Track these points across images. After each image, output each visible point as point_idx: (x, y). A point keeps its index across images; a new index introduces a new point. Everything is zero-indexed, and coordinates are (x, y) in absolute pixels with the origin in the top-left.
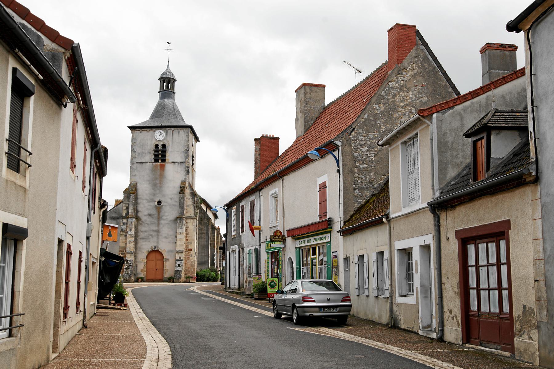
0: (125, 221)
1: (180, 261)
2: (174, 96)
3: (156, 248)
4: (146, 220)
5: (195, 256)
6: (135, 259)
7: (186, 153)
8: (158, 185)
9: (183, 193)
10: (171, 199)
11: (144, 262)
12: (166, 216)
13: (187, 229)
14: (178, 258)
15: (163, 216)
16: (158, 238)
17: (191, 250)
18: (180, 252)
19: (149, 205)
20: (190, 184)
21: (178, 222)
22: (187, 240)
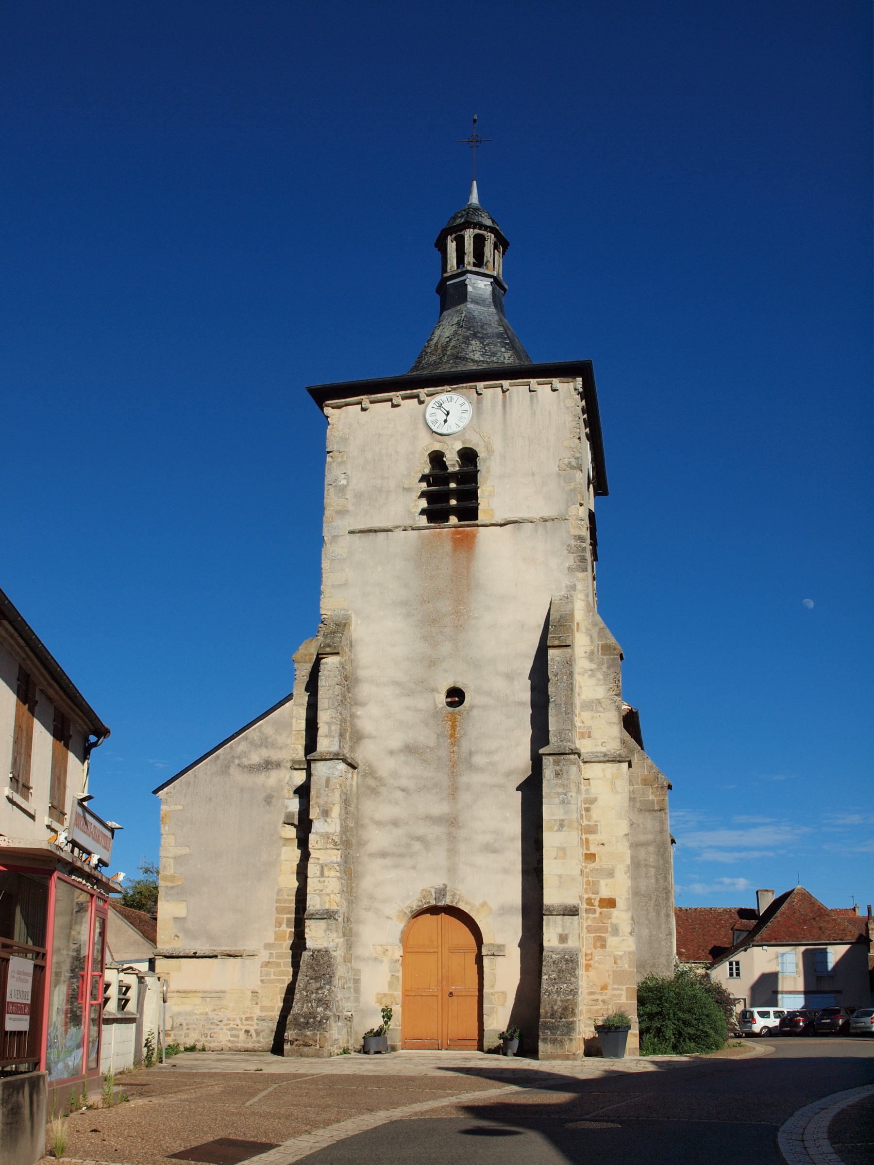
13: (587, 810)
16: (452, 852)
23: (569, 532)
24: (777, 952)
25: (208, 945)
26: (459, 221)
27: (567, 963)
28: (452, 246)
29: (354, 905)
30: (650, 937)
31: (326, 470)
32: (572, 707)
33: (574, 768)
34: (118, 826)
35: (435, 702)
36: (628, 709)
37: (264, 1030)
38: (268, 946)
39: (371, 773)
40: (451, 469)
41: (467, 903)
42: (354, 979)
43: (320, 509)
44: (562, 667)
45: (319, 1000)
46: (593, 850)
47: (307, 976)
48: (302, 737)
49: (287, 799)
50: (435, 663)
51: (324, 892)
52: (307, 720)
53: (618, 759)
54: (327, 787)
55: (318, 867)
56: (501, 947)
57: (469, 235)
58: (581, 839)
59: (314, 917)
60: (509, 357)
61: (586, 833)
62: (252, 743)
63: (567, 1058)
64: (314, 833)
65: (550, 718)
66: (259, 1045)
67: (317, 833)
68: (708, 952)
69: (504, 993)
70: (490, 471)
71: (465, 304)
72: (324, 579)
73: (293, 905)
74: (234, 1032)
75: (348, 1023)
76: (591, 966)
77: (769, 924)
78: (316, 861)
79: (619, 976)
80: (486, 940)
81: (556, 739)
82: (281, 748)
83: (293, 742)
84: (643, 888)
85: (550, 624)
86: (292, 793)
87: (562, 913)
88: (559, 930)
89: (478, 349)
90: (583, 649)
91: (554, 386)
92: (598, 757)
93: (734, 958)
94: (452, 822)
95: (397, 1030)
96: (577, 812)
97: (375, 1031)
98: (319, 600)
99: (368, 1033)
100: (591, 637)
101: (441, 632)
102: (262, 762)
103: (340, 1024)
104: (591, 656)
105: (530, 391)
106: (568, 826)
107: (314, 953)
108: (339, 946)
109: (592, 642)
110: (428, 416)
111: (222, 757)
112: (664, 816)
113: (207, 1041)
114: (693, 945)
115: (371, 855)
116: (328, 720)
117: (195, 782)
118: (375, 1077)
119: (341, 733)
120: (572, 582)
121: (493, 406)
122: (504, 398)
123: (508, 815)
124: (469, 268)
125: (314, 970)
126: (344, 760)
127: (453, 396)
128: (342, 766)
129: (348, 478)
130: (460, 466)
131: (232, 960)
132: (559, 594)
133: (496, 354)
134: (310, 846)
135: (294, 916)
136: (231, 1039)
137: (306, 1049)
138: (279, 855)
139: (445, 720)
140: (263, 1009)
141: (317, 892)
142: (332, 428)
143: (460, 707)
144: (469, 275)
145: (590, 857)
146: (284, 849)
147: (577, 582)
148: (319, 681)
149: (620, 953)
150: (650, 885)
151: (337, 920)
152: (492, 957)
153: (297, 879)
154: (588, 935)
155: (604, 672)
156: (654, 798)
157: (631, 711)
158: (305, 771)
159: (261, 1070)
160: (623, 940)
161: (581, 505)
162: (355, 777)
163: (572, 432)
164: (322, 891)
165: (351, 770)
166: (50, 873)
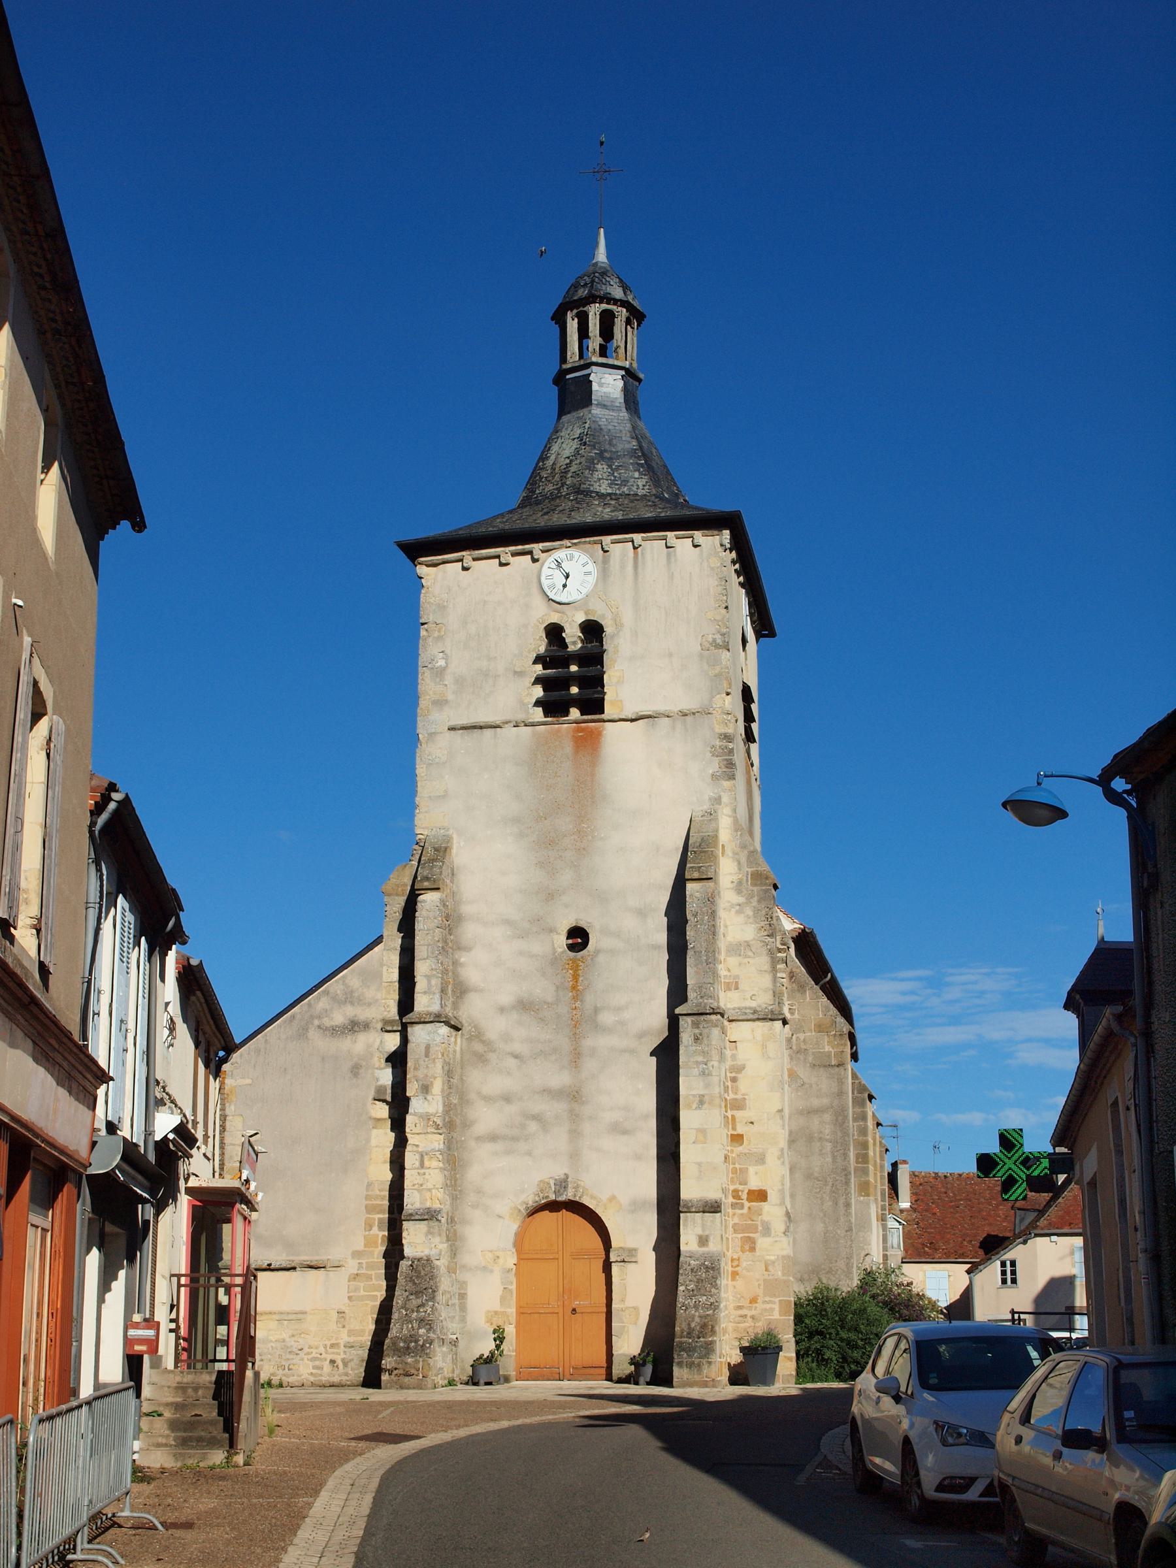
13: (734, 1080)
16: (575, 1134)
23: (713, 729)
24: (1072, 1245)
25: (284, 1255)
26: (583, 293)
27: (707, 1271)
28: (572, 325)
29: (458, 1201)
30: (825, 1234)
31: (420, 646)
32: (714, 955)
33: (716, 1032)
34: (263, 1150)
35: (553, 945)
36: (800, 928)
37: (353, 1360)
38: (356, 1254)
39: (478, 1035)
40: (571, 648)
41: (592, 1197)
42: (459, 1294)
43: (412, 697)
44: (702, 905)
45: (422, 1320)
46: (739, 1131)
47: (406, 1291)
48: (394, 991)
49: (377, 1069)
50: (553, 896)
51: (424, 1187)
52: (400, 968)
53: (769, 1017)
54: (427, 1055)
55: (417, 1157)
56: (632, 1252)
57: (594, 312)
58: (726, 1117)
59: (413, 1218)
60: (644, 486)
61: (732, 1109)
62: (335, 999)
63: (705, 1384)
64: (411, 1114)
65: (688, 969)
66: (346, 1378)
67: (415, 1114)
68: (978, 1244)
69: (636, 1308)
70: (618, 651)
71: (589, 409)
72: (419, 789)
73: (386, 1203)
74: (317, 1363)
75: (453, 1347)
76: (738, 1274)
77: (1060, 1200)
78: (415, 1148)
79: (771, 1287)
80: (615, 1243)
81: (695, 994)
82: (369, 1004)
83: (384, 997)
84: (817, 1169)
85: (690, 849)
86: (383, 1061)
87: (701, 1210)
88: (699, 1231)
89: (605, 476)
90: (730, 878)
91: (695, 541)
92: (746, 1014)
93: (1008, 1256)
94: (574, 1096)
95: (510, 1356)
96: (720, 1086)
97: (485, 1356)
98: (414, 816)
99: (477, 1359)
100: (739, 863)
101: (561, 856)
102: (347, 1022)
103: (444, 1349)
104: (739, 887)
105: (667, 547)
106: (709, 1103)
107: (413, 1262)
108: (443, 1253)
109: (740, 869)
110: (543, 578)
111: (298, 1016)
112: (843, 1073)
113: (284, 1375)
114: (954, 1234)
115: (478, 1139)
116: (428, 973)
117: (266, 1049)
118: (492, 1401)
119: (442, 988)
120: (716, 794)
121: (623, 567)
122: (636, 555)
123: (640, 1086)
124: (594, 359)
125: (415, 1284)
126: (447, 1023)
127: (574, 553)
128: (444, 1030)
129: (446, 658)
130: (582, 641)
131: (314, 1272)
132: (701, 808)
133: (628, 481)
134: (407, 1130)
135: (387, 1216)
136: (314, 1371)
137: (407, 1379)
138: (368, 1140)
139: (565, 968)
140: (351, 1333)
141: (416, 1186)
142: (427, 592)
143: (584, 951)
144: (594, 368)
145: (737, 1139)
146: (375, 1132)
147: (722, 794)
148: (416, 923)
149: (772, 1258)
150: (826, 1165)
151: (440, 1221)
152: (622, 1264)
153: (391, 1170)
154: (735, 1235)
155: (754, 907)
156: (831, 1049)
157: (804, 930)
158: (399, 1033)
159: (368, 1399)
160: (776, 1241)
161: (728, 694)
162: (459, 1040)
163: (717, 600)
164: (421, 1185)
165: (454, 1032)
166: (233, 1205)
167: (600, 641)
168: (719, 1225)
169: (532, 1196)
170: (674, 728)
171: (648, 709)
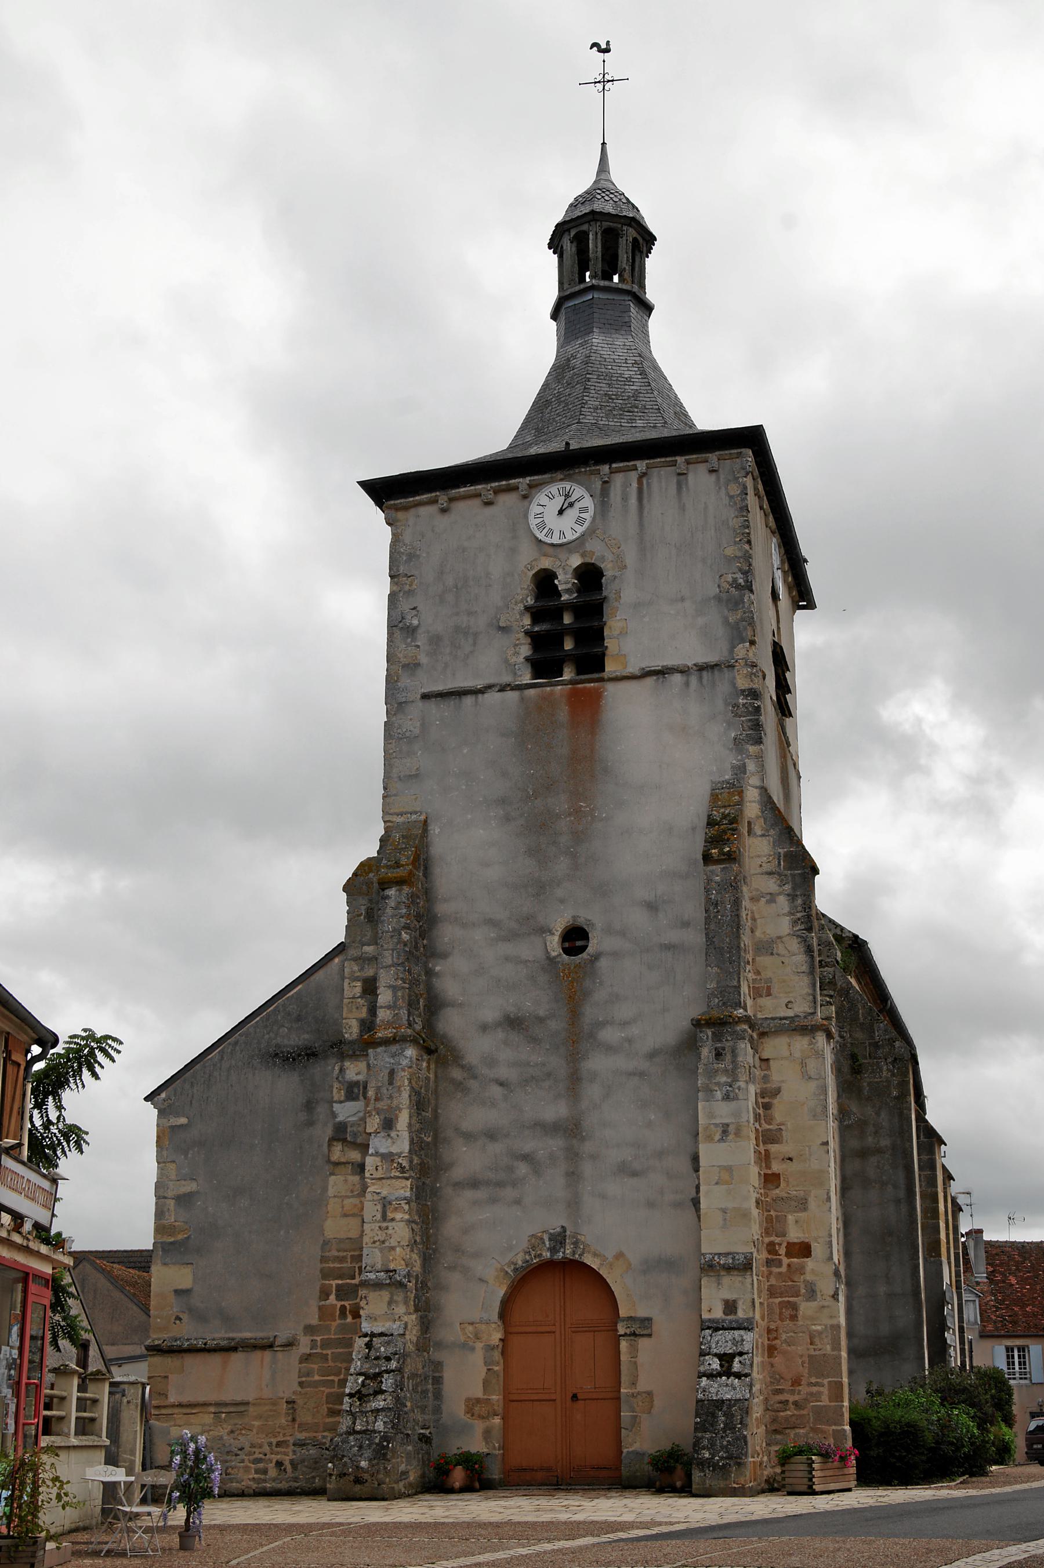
0: (354, 1070)
1: (729, 1335)
2: (645, 326)
3: (562, 1243)
4: (491, 1062)
5: (835, 1296)
6: (425, 1325)
7: (736, 604)
8: (563, 824)
9: (731, 858)
10: (652, 907)
11: (490, 1348)
12: (624, 1024)
13: (767, 1107)
14: (718, 1313)
15: (602, 1024)
16: (573, 1176)
17: (804, 1250)
18: (728, 1269)
19: (507, 959)
20: (767, 802)
21: (706, 1052)
22: (771, 1180)
40: (565, 597)
51: (387, 1244)
54: (391, 1083)
66: (297, 1485)
69: (650, 1394)
74: (261, 1465)
95: (496, 1456)
108: (409, 1327)
120: (738, 761)
121: (625, 498)
138: (325, 1189)
152: (632, 1338)
160: (823, 1307)
167: (599, 587)
168: (750, 1287)
169: (522, 1254)
170: (687, 684)
171: (656, 665)
